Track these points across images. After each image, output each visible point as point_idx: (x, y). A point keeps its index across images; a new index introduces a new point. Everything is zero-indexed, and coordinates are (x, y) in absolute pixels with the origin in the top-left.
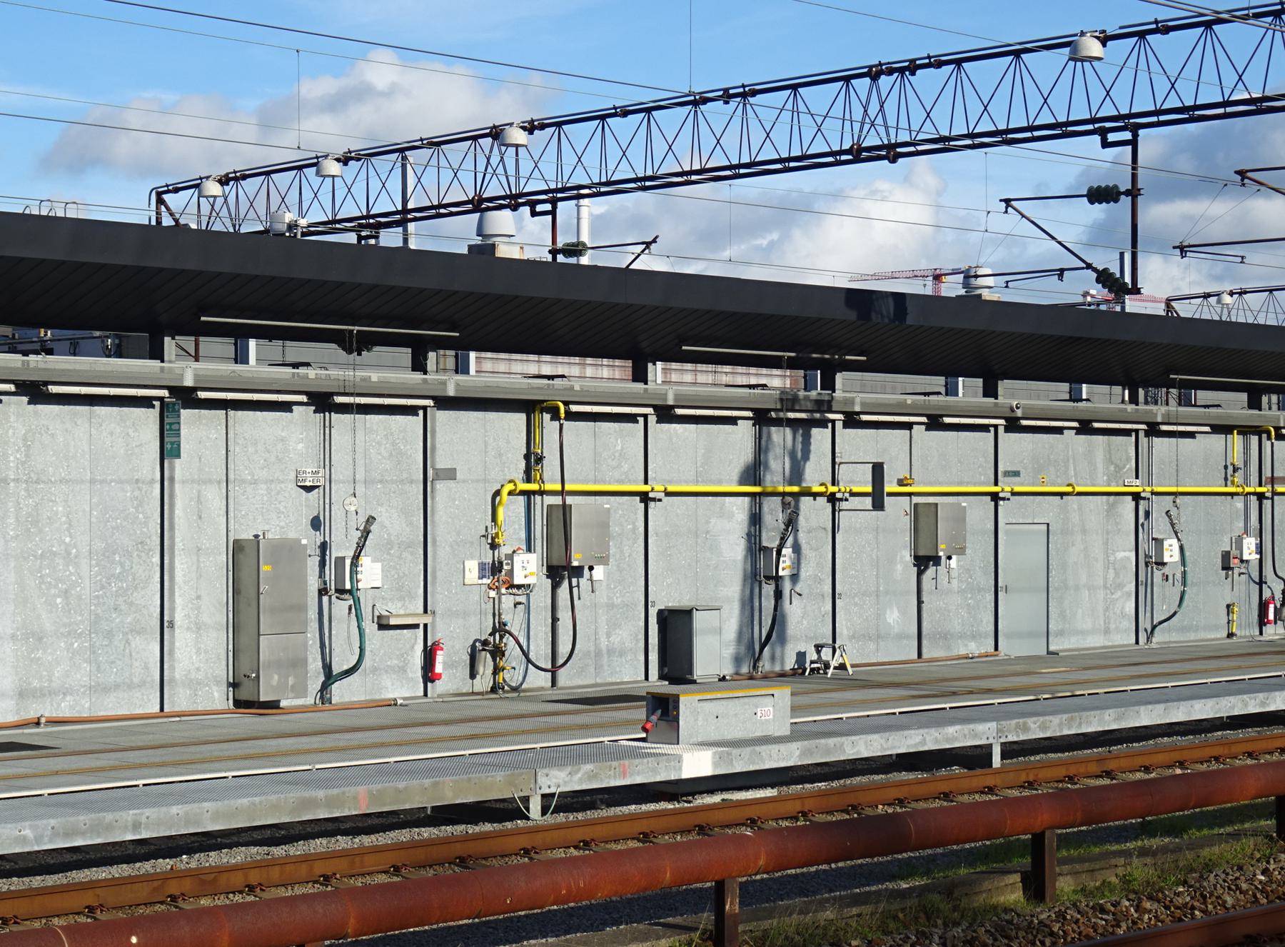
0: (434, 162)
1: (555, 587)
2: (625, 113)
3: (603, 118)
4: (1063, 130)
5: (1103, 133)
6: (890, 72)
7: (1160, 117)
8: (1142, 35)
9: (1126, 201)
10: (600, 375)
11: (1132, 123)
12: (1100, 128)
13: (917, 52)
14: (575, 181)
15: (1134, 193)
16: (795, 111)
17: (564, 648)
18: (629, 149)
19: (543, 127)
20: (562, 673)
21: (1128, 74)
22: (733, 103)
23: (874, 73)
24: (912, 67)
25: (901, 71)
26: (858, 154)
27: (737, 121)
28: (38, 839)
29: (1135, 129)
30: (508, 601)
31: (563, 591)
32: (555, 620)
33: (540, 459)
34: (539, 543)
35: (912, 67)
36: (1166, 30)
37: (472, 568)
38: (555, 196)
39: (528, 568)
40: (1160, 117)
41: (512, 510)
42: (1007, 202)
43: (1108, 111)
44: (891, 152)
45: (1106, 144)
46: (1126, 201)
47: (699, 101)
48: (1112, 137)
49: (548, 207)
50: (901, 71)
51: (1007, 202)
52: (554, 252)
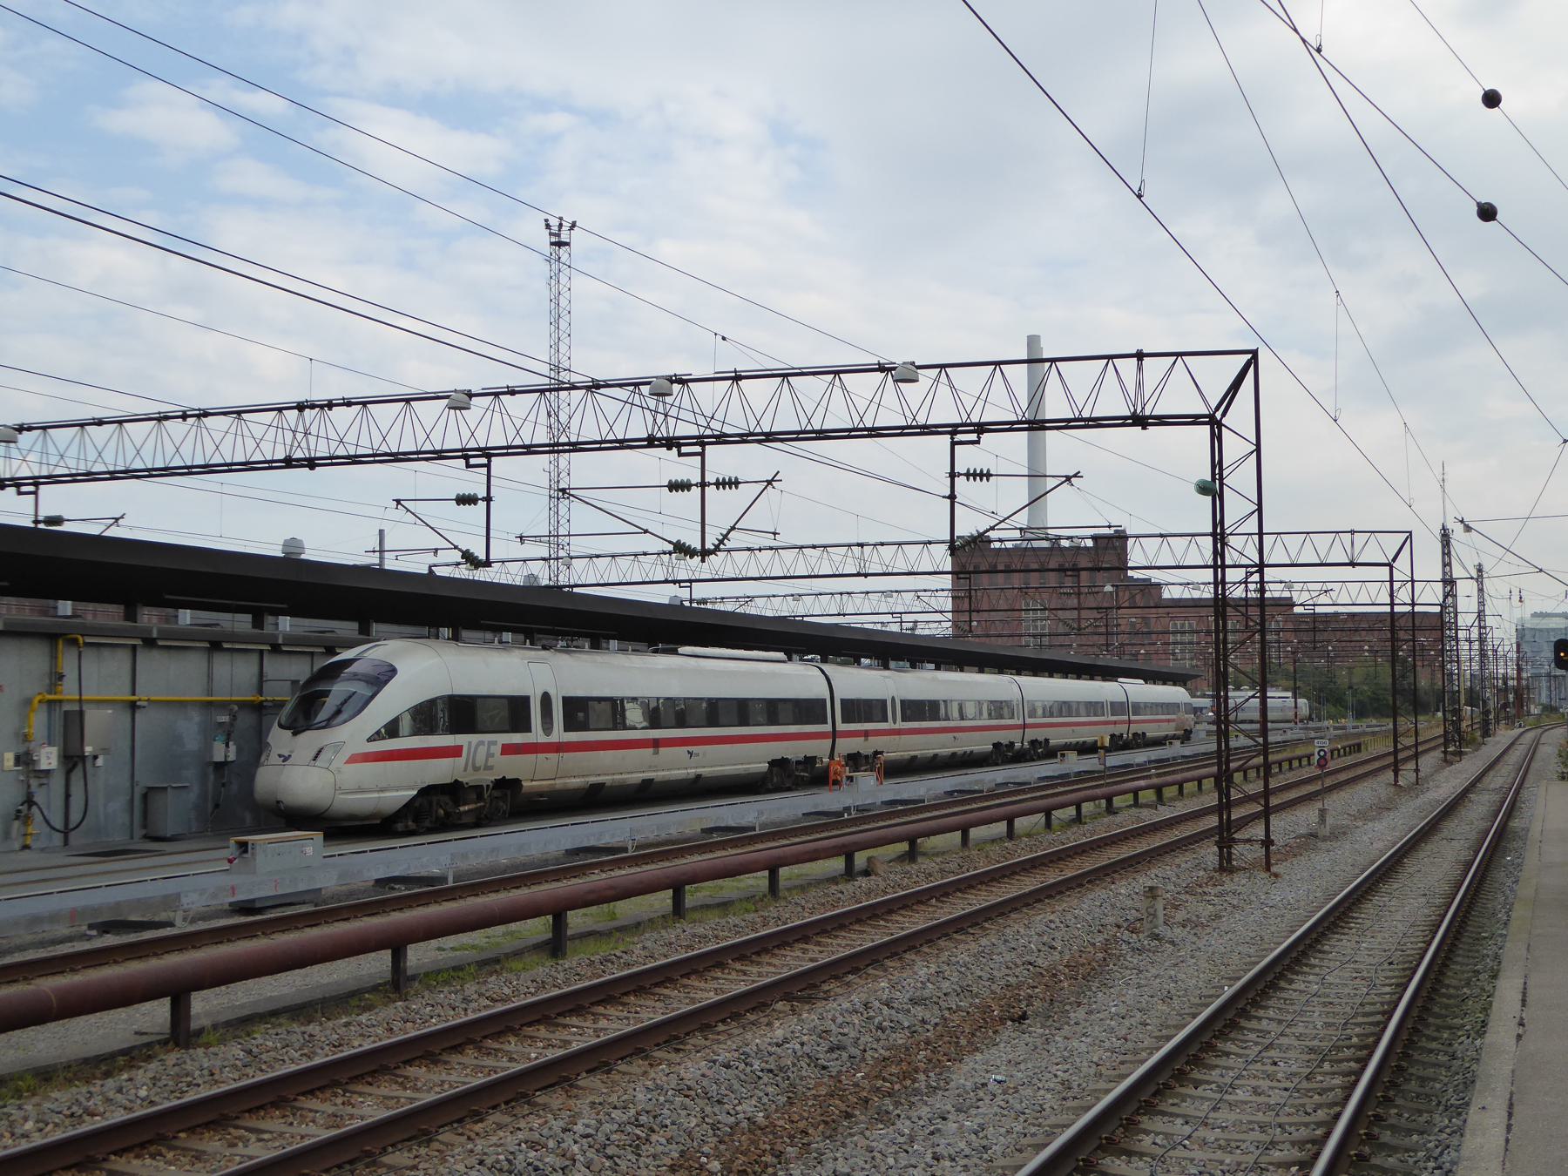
0: (233, 430)
1: (68, 773)
2: (100, 422)
3: (82, 425)
4: (439, 455)
5: (467, 458)
6: (312, 407)
7: (508, 450)
8: (496, 395)
9: (696, 491)
10: (108, 614)
11: (487, 453)
12: (465, 454)
13: (335, 394)
14: (134, 466)
15: (488, 499)
16: (82, 444)
17: (75, 817)
18: (105, 448)
19: (30, 429)
20: (72, 835)
21: (230, 437)
22: (190, 420)
23: (301, 407)
24: (330, 405)
25: (321, 407)
26: (289, 463)
27: (77, 439)
28: (567, 982)
29: (489, 456)
30: (34, 783)
31: (77, 776)
32: (68, 796)
33: (61, 677)
34: (59, 737)
35: (330, 405)
36: (512, 392)
37: (9, 759)
38: (37, 482)
39: (48, 758)
40: (508, 450)
41: (38, 722)
42: (398, 502)
43: (472, 444)
44: (311, 463)
45: (468, 466)
46: (482, 505)
47: (162, 418)
48: (473, 461)
49: (32, 488)
50: (321, 407)
51: (398, 502)
52: (36, 522)
